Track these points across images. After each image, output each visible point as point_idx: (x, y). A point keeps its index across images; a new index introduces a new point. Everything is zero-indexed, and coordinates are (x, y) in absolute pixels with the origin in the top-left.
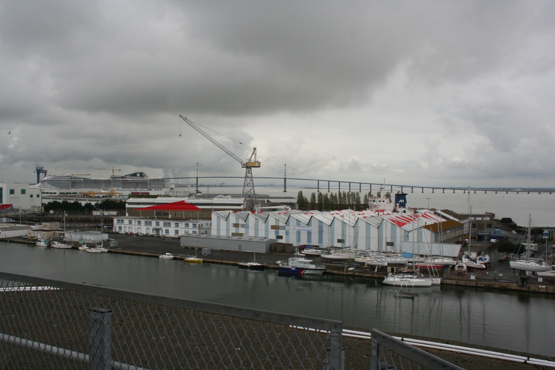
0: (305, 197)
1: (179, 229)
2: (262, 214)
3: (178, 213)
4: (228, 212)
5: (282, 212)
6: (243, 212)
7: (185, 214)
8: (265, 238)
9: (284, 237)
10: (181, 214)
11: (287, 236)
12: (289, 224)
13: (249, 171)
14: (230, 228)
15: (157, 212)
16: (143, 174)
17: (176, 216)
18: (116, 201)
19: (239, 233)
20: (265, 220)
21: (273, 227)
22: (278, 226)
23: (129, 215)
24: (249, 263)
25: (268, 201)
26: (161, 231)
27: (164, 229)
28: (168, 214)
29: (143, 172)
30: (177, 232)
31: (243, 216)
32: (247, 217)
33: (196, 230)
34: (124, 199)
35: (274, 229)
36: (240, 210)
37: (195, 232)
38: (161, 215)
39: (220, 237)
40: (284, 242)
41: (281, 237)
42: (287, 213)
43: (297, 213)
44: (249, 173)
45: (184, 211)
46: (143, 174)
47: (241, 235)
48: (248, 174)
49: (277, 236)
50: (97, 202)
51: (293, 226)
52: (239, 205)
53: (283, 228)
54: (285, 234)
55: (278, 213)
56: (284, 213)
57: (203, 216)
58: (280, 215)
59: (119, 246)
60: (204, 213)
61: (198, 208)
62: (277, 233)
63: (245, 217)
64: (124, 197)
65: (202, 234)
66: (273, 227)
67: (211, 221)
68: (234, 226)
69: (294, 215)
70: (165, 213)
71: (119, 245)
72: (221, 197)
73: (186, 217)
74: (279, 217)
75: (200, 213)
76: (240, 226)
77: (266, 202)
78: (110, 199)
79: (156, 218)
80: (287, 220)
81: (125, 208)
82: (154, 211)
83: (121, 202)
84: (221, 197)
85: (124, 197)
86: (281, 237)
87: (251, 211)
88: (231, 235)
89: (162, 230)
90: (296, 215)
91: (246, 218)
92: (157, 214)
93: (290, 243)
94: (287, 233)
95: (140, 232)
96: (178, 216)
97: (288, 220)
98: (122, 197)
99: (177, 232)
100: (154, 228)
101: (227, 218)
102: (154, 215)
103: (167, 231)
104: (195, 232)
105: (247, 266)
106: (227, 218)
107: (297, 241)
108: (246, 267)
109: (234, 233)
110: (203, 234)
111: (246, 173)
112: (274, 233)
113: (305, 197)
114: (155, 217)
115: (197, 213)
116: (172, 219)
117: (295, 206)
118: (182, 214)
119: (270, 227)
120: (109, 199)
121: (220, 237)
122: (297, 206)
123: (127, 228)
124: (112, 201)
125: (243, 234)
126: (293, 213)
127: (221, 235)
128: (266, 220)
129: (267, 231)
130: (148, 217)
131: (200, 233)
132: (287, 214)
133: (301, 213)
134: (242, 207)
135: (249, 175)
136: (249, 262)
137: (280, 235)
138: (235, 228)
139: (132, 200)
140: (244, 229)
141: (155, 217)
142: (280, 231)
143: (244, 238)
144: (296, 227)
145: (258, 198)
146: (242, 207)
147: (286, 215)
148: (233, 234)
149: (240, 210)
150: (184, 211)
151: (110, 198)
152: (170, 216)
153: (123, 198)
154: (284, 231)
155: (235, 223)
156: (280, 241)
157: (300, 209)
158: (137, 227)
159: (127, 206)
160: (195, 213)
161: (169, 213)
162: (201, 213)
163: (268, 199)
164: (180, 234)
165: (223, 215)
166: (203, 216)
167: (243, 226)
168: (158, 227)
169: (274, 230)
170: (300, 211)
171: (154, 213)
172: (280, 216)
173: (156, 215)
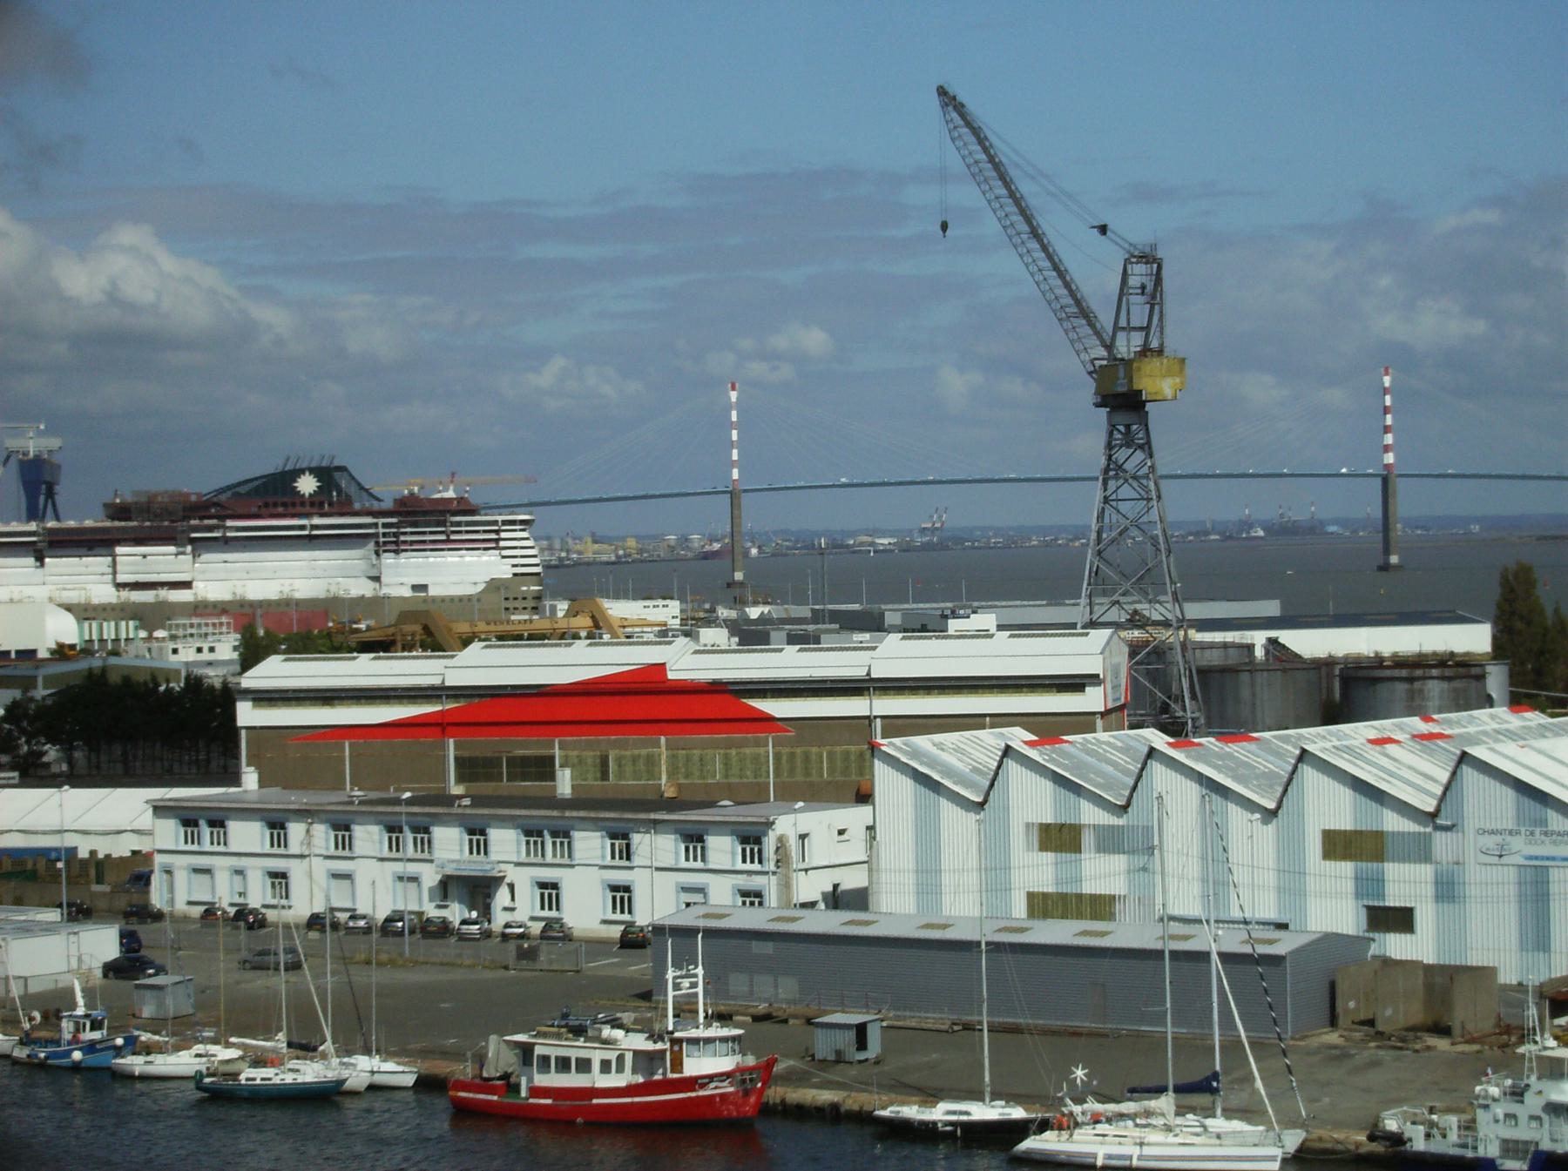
0: (1557, 611)
1: (638, 879)
2: (1252, 746)
3: (619, 760)
4: (990, 740)
5: (1400, 728)
6: (1102, 736)
7: (673, 760)
8: (1282, 926)
9: (1425, 917)
10: (641, 766)
11: (1447, 907)
12: (1460, 815)
13: (1128, 427)
14: (1015, 861)
15: (466, 754)
16: (337, 475)
17: (604, 775)
18: (158, 685)
19: (1080, 896)
20: (1278, 795)
21: (1338, 845)
22: (1379, 835)
23: (262, 783)
24: (943, 1106)
25: (1273, 642)
26: (502, 897)
27: (523, 879)
28: (543, 768)
29: (337, 463)
30: (621, 895)
31: (1110, 769)
32: (1139, 777)
33: (757, 882)
34: (210, 664)
35: (1345, 857)
36: (1082, 722)
37: (758, 894)
38: (502, 780)
39: (945, 926)
40: (1429, 958)
41: (1401, 920)
42: (1441, 736)
43: (1512, 735)
44: (1128, 446)
45: (663, 739)
46: (337, 475)
47: (1101, 907)
48: (1121, 455)
49: (1370, 909)
50: (16, 694)
51: (1493, 832)
52: (1074, 684)
53: (1419, 851)
54: (1430, 890)
55: (1373, 735)
56: (1414, 736)
57: (808, 774)
58: (1390, 748)
59: (200, 1016)
60: (814, 750)
61: (768, 719)
62: (1368, 886)
63: (1126, 772)
64: (212, 650)
65: (804, 905)
66: (1338, 845)
67: (867, 809)
68: (1044, 846)
69: (1492, 749)
70: (525, 761)
71: (199, 1006)
72: (87, 567)
73: (680, 787)
74: (1382, 769)
75: (785, 750)
76: (1088, 839)
77: (1259, 653)
78: (116, 667)
79: (460, 797)
80: (1439, 791)
81: (229, 730)
82: (444, 748)
83: (195, 684)
84: (87, 567)
85: (212, 650)
86: (1401, 920)
87: (1164, 729)
88: (1019, 909)
89: (511, 887)
90: (1510, 748)
91: (1131, 782)
92: (469, 769)
93: (1475, 959)
94: (1447, 890)
95: (348, 905)
96: (624, 781)
97: (1447, 788)
98: (199, 650)
99: (621, 895)
100: (449, 870)
101: (992, 785)
102: (443, 777)
103: (550, 891)
104: (758, 894)
105: (935, 1123)
106: (992, 785)
107: (1523, 947)
108: (926, 1133)
109: (1045, 895)
110: (812, 905)
111: (1109, 446)
112: (1349, 886)
113: (1557, 611)
114: (457, 790)
115: (762, 750)
116: (589, 806)
117: (1481, 678)
118: (652, 762)
119: (1314, 846)
120: (104, 670)
121: (945, 926)
122: (1496, 680)
123: (181, 877)
124: (127, 681)
125: (1112, 899)
126: (1485, 733)
127: (946, 912)
128: (1280, 789)
129: (1291, 880)
130: (408, 795)
131: (786, 901)
132: (1439, 742)
133: (1542, 732)
134: (1092, 700)
135: (1133, 460)
136: (942, 1099)
137: (1391, 902)
138: (1049, 857)
139: (274, 671)
140: (1118, 862)
141: (457, 790)
142: (1392, 870)
143: (1126, 933)
144: (1517, 843)
145: (1199, 630)
146: (1092, 700)
147: (1431, 753)
148: (1041, 905)
149: (1082, 722)
150: (663, 739)
151: (113, 660)
152: (565, 783)
153: (206, 656)
154: (1425, 872)
155: (1049, 820)
156: (1396, 946)
157: (1517, 702)
158: (321, 867)
159: (247, 715)
160: (748, 751)
161: (552, 758)
162: (792, 755)
163: (1273, 634)
164: (643, 917)
165: (959, 765)
166: (808, 774)
167: (1110, 842)
168: (475, 866)
169: (1347, 868)
170: (1535, 718)
171: (444, 758)
172: (1384, 762)
173: (461, 779)
